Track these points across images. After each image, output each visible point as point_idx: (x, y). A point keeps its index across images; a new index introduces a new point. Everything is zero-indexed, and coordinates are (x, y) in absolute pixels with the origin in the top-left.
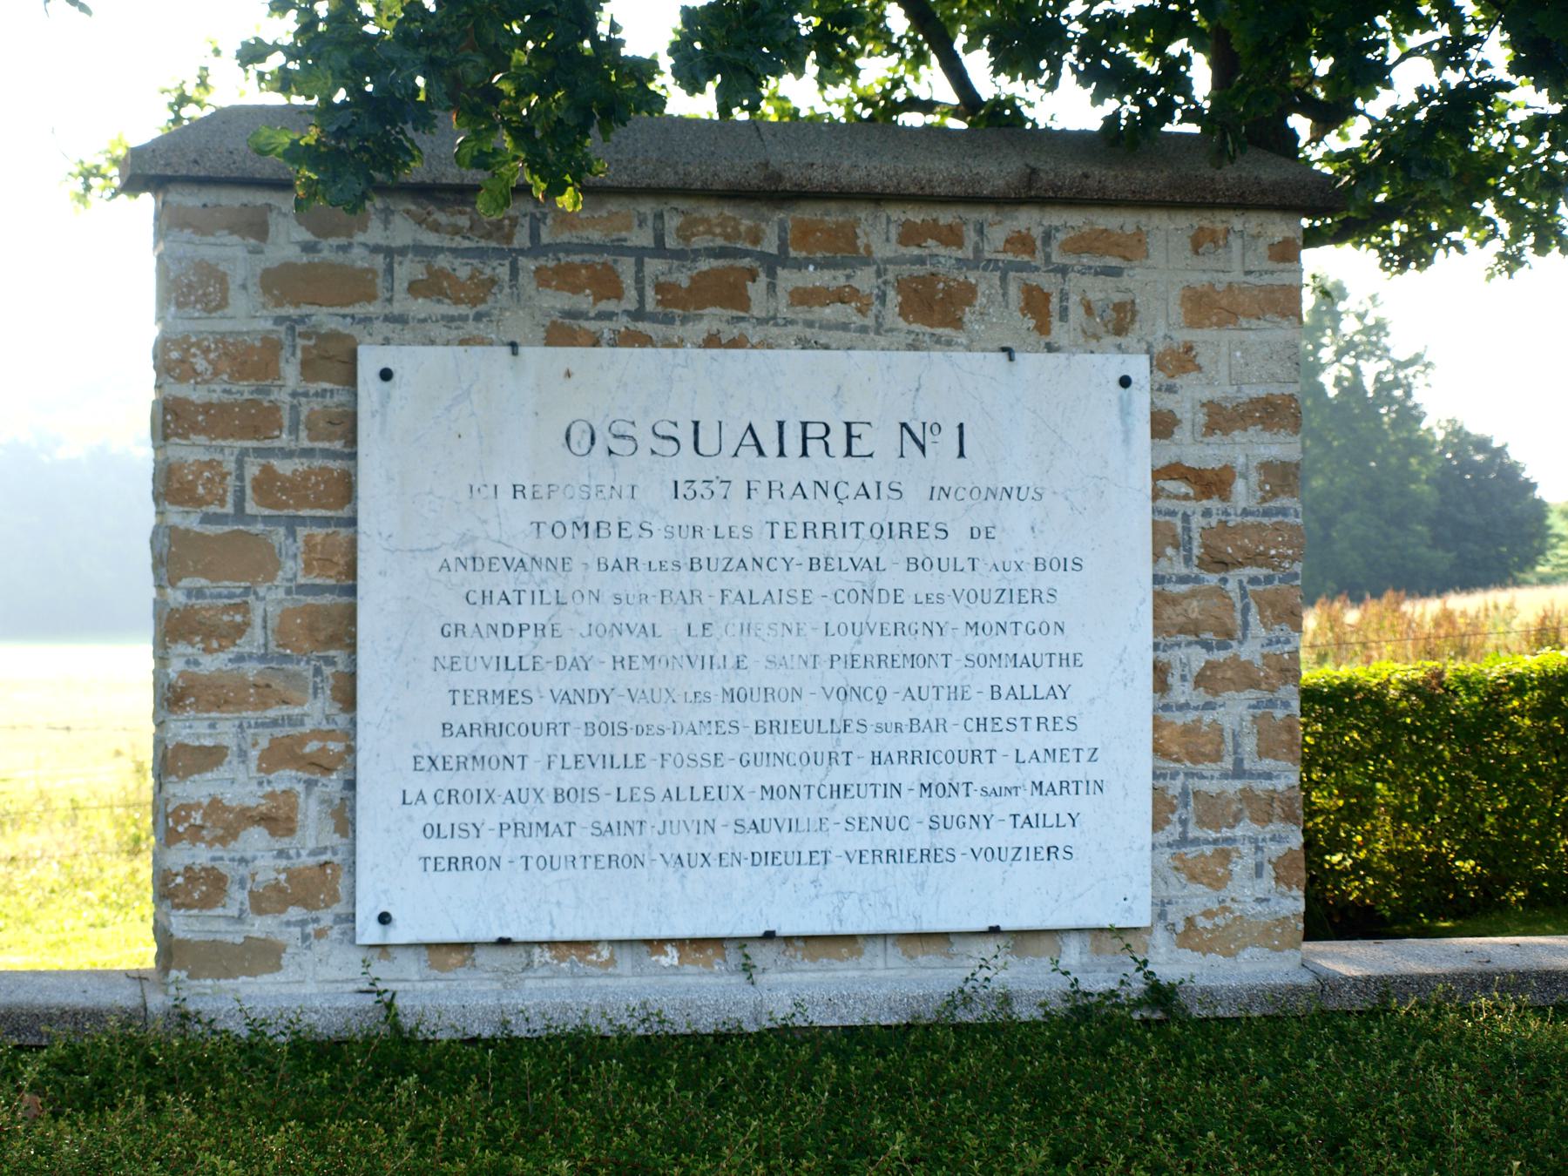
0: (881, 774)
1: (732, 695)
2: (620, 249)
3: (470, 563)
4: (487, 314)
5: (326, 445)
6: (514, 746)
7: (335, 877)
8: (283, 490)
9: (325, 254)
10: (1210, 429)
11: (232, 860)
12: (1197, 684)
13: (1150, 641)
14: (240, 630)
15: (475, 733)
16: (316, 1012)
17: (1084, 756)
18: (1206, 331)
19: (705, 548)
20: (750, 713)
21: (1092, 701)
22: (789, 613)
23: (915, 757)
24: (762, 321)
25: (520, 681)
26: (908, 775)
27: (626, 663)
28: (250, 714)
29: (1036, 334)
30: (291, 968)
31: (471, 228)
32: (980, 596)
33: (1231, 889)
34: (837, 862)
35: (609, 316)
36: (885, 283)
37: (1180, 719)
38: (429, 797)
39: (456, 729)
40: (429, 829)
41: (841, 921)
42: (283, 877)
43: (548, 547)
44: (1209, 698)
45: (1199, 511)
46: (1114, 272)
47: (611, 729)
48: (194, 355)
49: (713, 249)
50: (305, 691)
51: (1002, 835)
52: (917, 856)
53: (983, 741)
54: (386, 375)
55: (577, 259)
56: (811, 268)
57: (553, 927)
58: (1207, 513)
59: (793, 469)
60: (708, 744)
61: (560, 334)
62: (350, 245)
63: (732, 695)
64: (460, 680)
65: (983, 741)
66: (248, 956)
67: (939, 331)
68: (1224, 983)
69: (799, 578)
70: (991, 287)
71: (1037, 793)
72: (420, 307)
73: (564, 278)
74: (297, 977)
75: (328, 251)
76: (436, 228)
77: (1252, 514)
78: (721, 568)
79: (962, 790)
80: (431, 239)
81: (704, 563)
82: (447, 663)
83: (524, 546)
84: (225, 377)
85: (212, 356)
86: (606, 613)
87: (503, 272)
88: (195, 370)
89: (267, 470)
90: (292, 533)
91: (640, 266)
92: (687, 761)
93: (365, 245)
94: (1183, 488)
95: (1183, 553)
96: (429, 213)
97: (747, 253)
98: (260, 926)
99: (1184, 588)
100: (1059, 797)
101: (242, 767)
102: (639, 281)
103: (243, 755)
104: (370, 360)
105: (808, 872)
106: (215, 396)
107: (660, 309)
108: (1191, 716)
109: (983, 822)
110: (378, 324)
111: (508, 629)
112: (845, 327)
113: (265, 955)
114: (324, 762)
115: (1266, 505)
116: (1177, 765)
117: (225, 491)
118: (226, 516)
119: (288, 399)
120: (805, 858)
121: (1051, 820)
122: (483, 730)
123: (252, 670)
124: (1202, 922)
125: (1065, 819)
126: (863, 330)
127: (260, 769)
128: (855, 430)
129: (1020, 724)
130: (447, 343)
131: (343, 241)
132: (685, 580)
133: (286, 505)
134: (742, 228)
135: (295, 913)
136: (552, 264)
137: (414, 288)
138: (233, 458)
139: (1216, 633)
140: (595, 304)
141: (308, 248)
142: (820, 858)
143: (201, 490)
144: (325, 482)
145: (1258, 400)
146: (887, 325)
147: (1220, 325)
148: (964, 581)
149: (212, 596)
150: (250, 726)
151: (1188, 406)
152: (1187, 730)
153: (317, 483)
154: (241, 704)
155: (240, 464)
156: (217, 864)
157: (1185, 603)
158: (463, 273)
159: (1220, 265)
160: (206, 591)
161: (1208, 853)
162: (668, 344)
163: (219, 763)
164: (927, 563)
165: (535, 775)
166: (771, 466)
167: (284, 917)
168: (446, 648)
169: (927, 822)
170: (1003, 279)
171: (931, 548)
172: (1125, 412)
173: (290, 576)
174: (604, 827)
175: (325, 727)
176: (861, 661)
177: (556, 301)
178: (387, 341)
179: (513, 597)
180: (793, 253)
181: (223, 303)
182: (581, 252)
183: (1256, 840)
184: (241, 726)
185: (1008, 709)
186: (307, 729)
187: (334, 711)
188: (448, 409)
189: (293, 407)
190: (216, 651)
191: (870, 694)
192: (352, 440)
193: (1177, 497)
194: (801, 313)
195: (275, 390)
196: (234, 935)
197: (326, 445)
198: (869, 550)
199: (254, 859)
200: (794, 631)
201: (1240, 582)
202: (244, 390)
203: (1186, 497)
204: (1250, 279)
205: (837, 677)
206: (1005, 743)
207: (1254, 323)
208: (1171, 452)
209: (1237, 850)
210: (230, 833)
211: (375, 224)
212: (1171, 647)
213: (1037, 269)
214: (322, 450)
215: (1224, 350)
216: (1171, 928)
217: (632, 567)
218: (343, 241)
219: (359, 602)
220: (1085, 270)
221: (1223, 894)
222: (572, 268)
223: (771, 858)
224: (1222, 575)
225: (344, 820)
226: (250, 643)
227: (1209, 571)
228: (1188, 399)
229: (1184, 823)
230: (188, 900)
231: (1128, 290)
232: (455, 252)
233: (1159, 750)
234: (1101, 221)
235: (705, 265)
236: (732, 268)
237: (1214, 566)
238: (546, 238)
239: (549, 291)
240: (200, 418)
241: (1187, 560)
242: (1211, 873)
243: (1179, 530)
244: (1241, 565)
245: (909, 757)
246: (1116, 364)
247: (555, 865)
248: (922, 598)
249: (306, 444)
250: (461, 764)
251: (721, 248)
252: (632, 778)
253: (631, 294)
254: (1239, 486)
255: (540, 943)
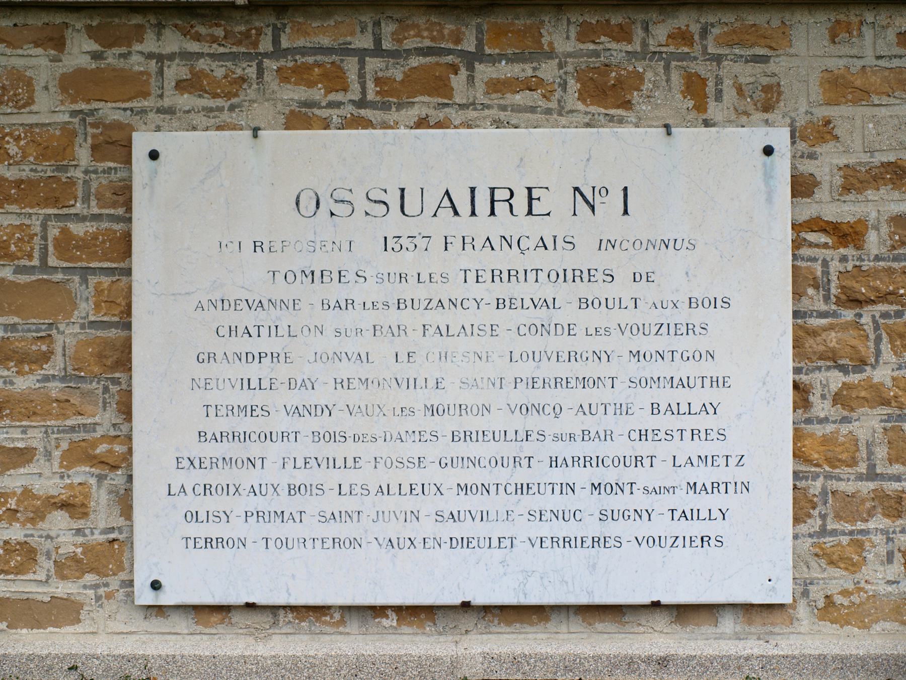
0: (558, 475)
1: (433, 411)
2: (346, 51)
3: (219, 304)
4: (239, 106)
5: (112, 211)
6: (255, 450)
7: (121, 552)
8: (78, 247)
9: (110, 60)
10: (847, 188)
11: (41, 536)
12: (835, 402)
13: (790, 365)
14: (46, 357)
15: (225, 439)
16: (98, 658)
17: (733, 461)
18: (843, 107)
19: (409, 291)
20: (446, 425)
21: (739, 416)
22: (483, 343)
23: (586, 462)
24: (462, 107)
25: (258, 398)
26: (581, 476)
27: (345, 384)
28: (53, 422)
29: (694, 113)
30: (88, 622)
31: (225, 37)
32: (641, 329)
33: (866, 572)
34: (521, 547)
35: (337, 105)
36: (566, 73)
37: (819, 430)
38: (189, 490)
39: (209, 436)
40: (189, 515)
41: (525, 595)
42: (79, 550)
43: (282, 291)
44: (845, 413)
45: (837, 257)
46: (764, 59)
47: (333, 437)
48: (8, 142)
49: (421, 49)
50: (96, 405)
51: (662, 526)
52: (589, 542)
53: (644, 448)
54: (154, 155)
55: (310, 60)
56: (504, 62)
57: (290, 595)
58: (844, 259)
59: (483, 226)
60: (412, 450)
61: (299, 119)
62: (130, 53)
63: (433, 411)
64: (213, 397)
65: (644, 448)
66: (55, 612)
67: (612, 112)
68: (854, 652)
69: (488, 315)
70: (656, 74)
71: (691, 492)
72: (185, 101)
73: (298, 75)
74: (91, 630)
75: (112, 58)
76: (198, 38)
77: (883, 259)
78: (423, 307)
79: (627, 489)
80: (194, 47)
81: (409, 303)
82: (202, 384)
83: (264, 290)
84: (32, 159)
85: (22, 143)
86: (328, 343)
87: (252, 72)
88: (8, 154)
89: (65, 231)
90: (85, 281)
91: (362, 63)
92: (395, 463)
93: (141, 53)
94: (823, 239)
95: (822, 292)
96: (192, 26)
97: (449, 52)
98: (62, 589)
99: (824, 321)
100: (710, 495)
101: (47, 463)
102: (361, 76)
103: (48, 455)
104: (142, 142)
105: (497, 554)
106: (24, 174)
107: (378, 98)
108: (830, 428)
109: (645, 516)
110: (151, 115)
111: (250, 356)
112: (532, 110)
113: (64, 612)
114: (110, 461)
115: (896, 252)
116: (817, 469)
117: (32, 249)
118: (34, 267)
119: (81, 175)
120: (495, 543)
121: (704, 514)
122: (231, 437)
123: (55, 388)
124: (839, 599)
125: (716, 514)
126: (548, 111)
127: (61, 467)
128: (535, 194)
129: (677, 435)
130: (207, 129)
131: (124, 50)
132: (393, 317)
133: (80, 259)
134: (446, 32)
135: (90, 578)
136: (290, 64)
137: (180, 86)
138: (38, 223)
139: (851, 359)
140: (326, 96)
141: (96, 56)
142: (507, 543)
143: (13, 248)
144: (110, 241)
145: (889, 164)
146: (569, 107)
147: (855, 102)
148: (628, 317)
149: (23, 331)
150: (53, 433)
151: (827, 170)
152: (826, 440)
153: (104, 242)
154: (48, 414)
155: (44, 226)
156: (29, 539)
157: (824, 335)
158: (219, 73)
159: (854, 52)
160: (839, 329)
161: (844, 543)
162: (385, 126)
163: (30, 461)
164: (596, 302)
165: (272, 474)
166: (464, 225)
167: (81, 582)
168: (201, 371)
169: (598, 515)
170: (667, 68)
171: (598, 290)
172: (768, 176)
173: (84, 315)
174: (328, 516)
175: (112, 433)
176: (540, 383)
177: (295, 93)
178: (158, 129)
179: (253, 331)
180: (488, 51)
181: (30, 101)
182: (315, 55)
183: (887, 533)
184: (46, 432)
185: (665, 422)
186: (98, 435)
187: (118, 421)
188: (202, 182)
189: (85, 182)
190: (27, 373)
191: (548, 409)
192: (129, 209)
193: (817, 246)
194: (495, 99)
195: (72, 169)
196: (42, 593)
197: (112, 211)
198: (546, 290)
199: (58, 536)
200: (484, 358)
201: (873, 317)
202: (46, 169)
203: (825, 246)
204: (882, 63)
205: (523, 395)
206: (664, 450)
207: (885, 100)
208: (809, 210)
209: (870, 541)
210: (38, 516)
211: (150, 36)
212: (813, 371)
213: (696, 58)
214: (107, 215)
215: (858, 122)
216: (812, 604)
217: (350, 306)
218: (124, 50)
219: (133, 335)
220: (737, 58)
221: (858, 576)
222: (308, 68)
223: (466, 542)
224: (857, 310)
225: (125, 503)
226: (54, 367)
227: (846, 307)
228: (827, 164)
229: (823, 517)
230: (6, 568)
231: (774, 75)
232: (213, 56)
233: (798, 455)
234: (750, 18)
235: (415, 62)
236: (437, 64)
237: (851, 304)
238: (285, 44)
239: (289, 86)
240: (13, 191)
241: (827, 299)
242: (847, 560)
243: (819, 273)
244: (873, 302)
245: (582, 461)
246: (760, 136)
247: (290, 546)
248: (592, 331)
249: (96, 211)
250: (214, 463)
251: (428, 47)
252: (348, 477)
253: (356, 86)
254: (872, 237)
255: (284, 607)
